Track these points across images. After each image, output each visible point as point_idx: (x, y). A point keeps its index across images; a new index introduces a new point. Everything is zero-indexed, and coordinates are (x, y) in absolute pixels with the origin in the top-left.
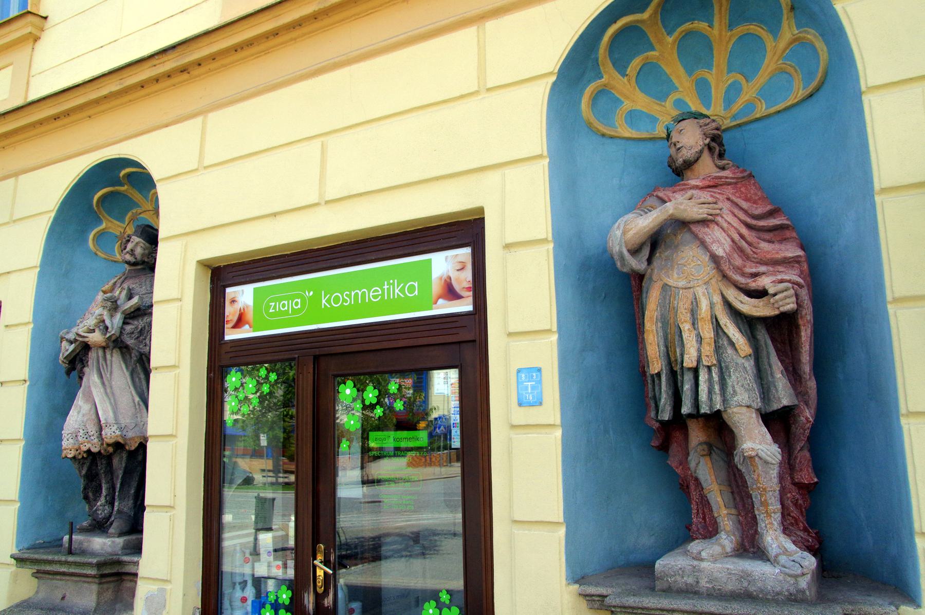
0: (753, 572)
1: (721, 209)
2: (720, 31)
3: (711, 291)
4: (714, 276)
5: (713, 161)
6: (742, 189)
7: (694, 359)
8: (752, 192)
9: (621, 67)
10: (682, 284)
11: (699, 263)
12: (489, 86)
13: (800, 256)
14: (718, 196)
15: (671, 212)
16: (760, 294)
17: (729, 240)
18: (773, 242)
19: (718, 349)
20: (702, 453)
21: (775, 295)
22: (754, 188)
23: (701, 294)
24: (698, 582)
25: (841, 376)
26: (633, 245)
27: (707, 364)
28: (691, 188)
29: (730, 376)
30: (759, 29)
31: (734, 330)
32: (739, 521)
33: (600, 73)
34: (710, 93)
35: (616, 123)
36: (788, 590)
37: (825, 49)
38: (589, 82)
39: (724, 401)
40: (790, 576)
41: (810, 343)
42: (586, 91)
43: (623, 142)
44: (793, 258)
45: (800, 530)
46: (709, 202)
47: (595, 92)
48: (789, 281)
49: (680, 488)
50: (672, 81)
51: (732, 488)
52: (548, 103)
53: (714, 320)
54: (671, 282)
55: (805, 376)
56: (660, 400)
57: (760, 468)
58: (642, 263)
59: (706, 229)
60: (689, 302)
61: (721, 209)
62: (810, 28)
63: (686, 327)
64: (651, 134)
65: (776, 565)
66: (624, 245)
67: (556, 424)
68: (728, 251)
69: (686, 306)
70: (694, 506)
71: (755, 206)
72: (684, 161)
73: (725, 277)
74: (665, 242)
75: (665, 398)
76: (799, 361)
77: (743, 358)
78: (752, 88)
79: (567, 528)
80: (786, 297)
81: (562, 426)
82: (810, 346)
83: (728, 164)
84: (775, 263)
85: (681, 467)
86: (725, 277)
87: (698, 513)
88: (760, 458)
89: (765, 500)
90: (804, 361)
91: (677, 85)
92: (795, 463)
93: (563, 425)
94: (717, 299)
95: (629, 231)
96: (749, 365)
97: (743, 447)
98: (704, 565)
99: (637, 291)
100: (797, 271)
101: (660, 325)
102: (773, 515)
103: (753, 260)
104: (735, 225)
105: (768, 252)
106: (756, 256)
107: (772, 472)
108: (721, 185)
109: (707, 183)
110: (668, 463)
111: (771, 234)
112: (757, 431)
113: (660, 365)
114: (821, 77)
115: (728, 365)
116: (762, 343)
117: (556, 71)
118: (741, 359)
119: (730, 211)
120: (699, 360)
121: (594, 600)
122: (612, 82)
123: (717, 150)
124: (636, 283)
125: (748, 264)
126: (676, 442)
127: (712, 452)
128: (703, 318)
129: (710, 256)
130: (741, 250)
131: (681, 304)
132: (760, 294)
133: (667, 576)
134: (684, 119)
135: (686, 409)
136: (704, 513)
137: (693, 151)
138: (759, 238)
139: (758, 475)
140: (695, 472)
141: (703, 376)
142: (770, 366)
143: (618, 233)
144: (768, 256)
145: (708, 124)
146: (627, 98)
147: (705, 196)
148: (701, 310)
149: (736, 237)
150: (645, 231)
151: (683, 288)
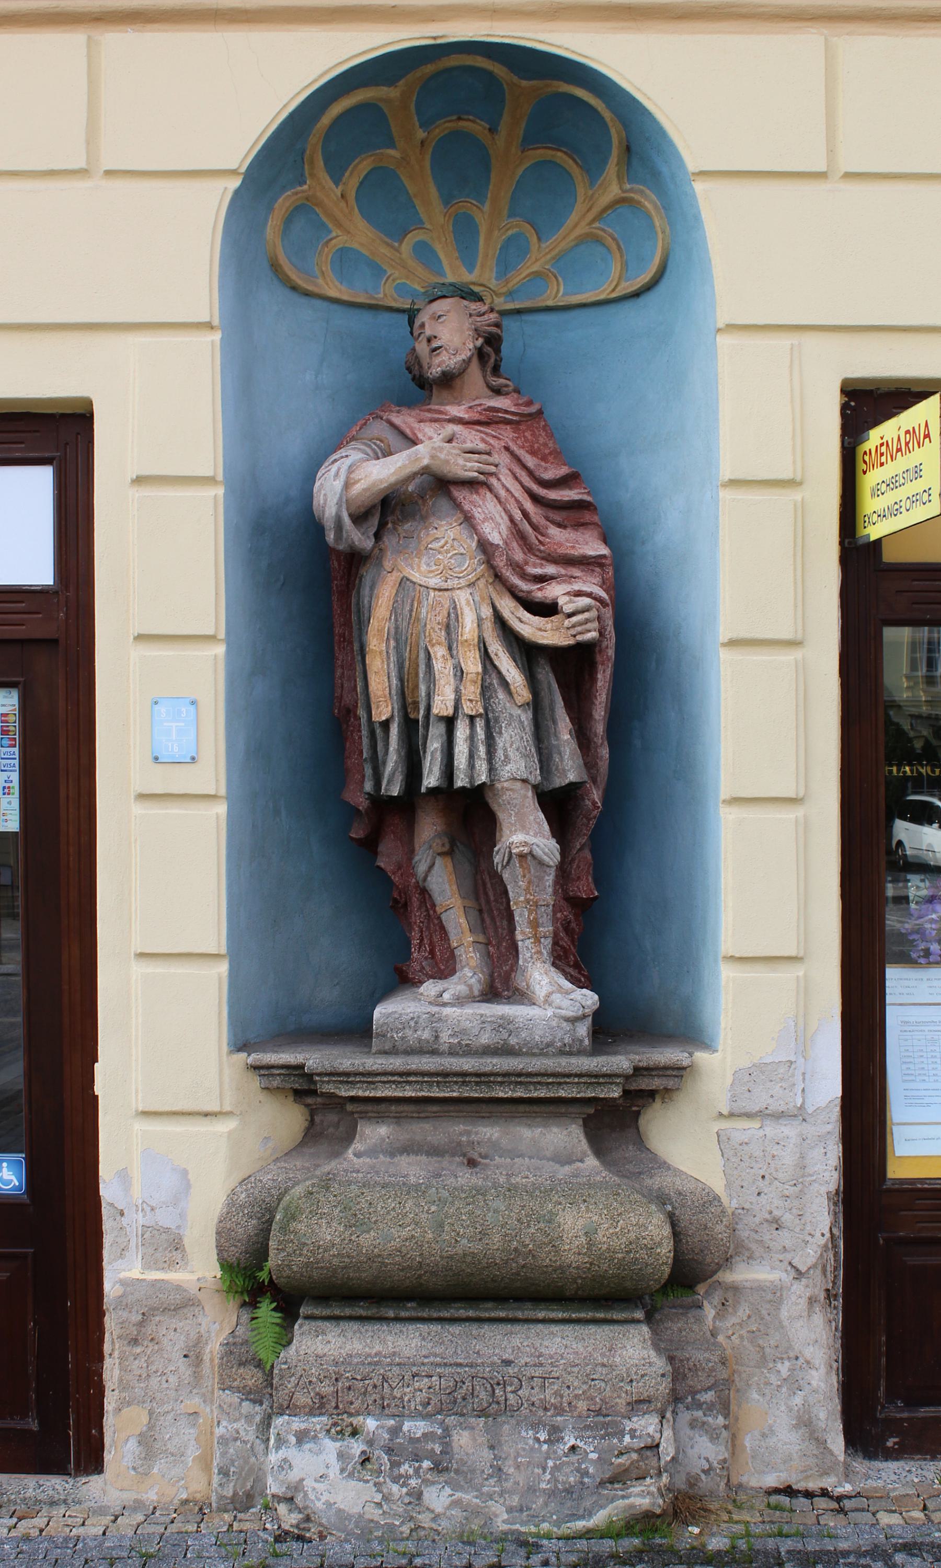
4: (483, 575)
5: (484, 377)
6: (526, 434)
8: (541, 440)
9: (337, 174)
10: (434, 582)
11: (462, 551)
13: (604, 556)
14: (492, 441)
15: (426, 462)
16: (547, 609)
17: (506, 518)
18: (565, 527)
19: (486, 691)
20: (440, 850)
21: (570, 616)
23: (463, 602)
24: (437, 1037)
25: (637, 743)
26: (359, 507)
27: (470, 713)
29: (500, 733)
30: (571, 162)
33: (302, 175)
34: (477, 242)
36: (562, 1040)
37: (600, 102)
39: (491, 769)
41: (608, 690)
43: (325, 304)
44: (594, 557)
45: (570, 966)
47: (291, 209)
48: (589, 595)
51: (480, 905)
52: (224, 227)
53: (482, 645)
54: (416, 576)
55: (595, 739)
56: (384, 763)
58: (368, 537)
61: (496, 466)
64: (373, 298)
66: (344, 506)
67: (219, 794)
68: (505, 537)
69: (439, 618)
71: (543, 464)
72: (444, 373)
73: (498, 577)
75: (396, 762)
76: (590, 716)
77: (520, 707)
78: (547, 254)
79: (230, 964)
81: (227, 798)
82: (607, 695)
83: (507, 386)
87: (421, 944)
88: (533, 856)
90: (597, 717)
91: (423, 216)
94: (487, 612)
96: (527, 718)
100: (598, 580)
102: (542, 940)
103: (538, 553)
104: (517, 495)
106: (542, 548)
107: (547, 878)
109: (476, 417)
110: (378, 867)
111: (564, 514)
112: (532, 818)
113: (390, 708)
115: (499, 717)
116: (545, 686)
117: (243, 169)
119: (510, 470)
120: (457, 706)
121: (273, 1075)
123: (492, 360)
124: (339, 565)
125: (533, 559)
127: (455, 848)
128: (466, 641)
129: (479, 541)
130: (521, 536)
132: (547, 609)
134: (444, 297)
135: (431, 779)
136: (431, 944)
137: (460, 358)
138: (547, 519)
140: (425, 879)
141: (461, 731)
143: (338, 484)
144: (561, 551)
145: (484, 314)
146: (339, 225)
147: (472, 438)
149: (518, 515)
150: (382, 486)
151: (435, 589)
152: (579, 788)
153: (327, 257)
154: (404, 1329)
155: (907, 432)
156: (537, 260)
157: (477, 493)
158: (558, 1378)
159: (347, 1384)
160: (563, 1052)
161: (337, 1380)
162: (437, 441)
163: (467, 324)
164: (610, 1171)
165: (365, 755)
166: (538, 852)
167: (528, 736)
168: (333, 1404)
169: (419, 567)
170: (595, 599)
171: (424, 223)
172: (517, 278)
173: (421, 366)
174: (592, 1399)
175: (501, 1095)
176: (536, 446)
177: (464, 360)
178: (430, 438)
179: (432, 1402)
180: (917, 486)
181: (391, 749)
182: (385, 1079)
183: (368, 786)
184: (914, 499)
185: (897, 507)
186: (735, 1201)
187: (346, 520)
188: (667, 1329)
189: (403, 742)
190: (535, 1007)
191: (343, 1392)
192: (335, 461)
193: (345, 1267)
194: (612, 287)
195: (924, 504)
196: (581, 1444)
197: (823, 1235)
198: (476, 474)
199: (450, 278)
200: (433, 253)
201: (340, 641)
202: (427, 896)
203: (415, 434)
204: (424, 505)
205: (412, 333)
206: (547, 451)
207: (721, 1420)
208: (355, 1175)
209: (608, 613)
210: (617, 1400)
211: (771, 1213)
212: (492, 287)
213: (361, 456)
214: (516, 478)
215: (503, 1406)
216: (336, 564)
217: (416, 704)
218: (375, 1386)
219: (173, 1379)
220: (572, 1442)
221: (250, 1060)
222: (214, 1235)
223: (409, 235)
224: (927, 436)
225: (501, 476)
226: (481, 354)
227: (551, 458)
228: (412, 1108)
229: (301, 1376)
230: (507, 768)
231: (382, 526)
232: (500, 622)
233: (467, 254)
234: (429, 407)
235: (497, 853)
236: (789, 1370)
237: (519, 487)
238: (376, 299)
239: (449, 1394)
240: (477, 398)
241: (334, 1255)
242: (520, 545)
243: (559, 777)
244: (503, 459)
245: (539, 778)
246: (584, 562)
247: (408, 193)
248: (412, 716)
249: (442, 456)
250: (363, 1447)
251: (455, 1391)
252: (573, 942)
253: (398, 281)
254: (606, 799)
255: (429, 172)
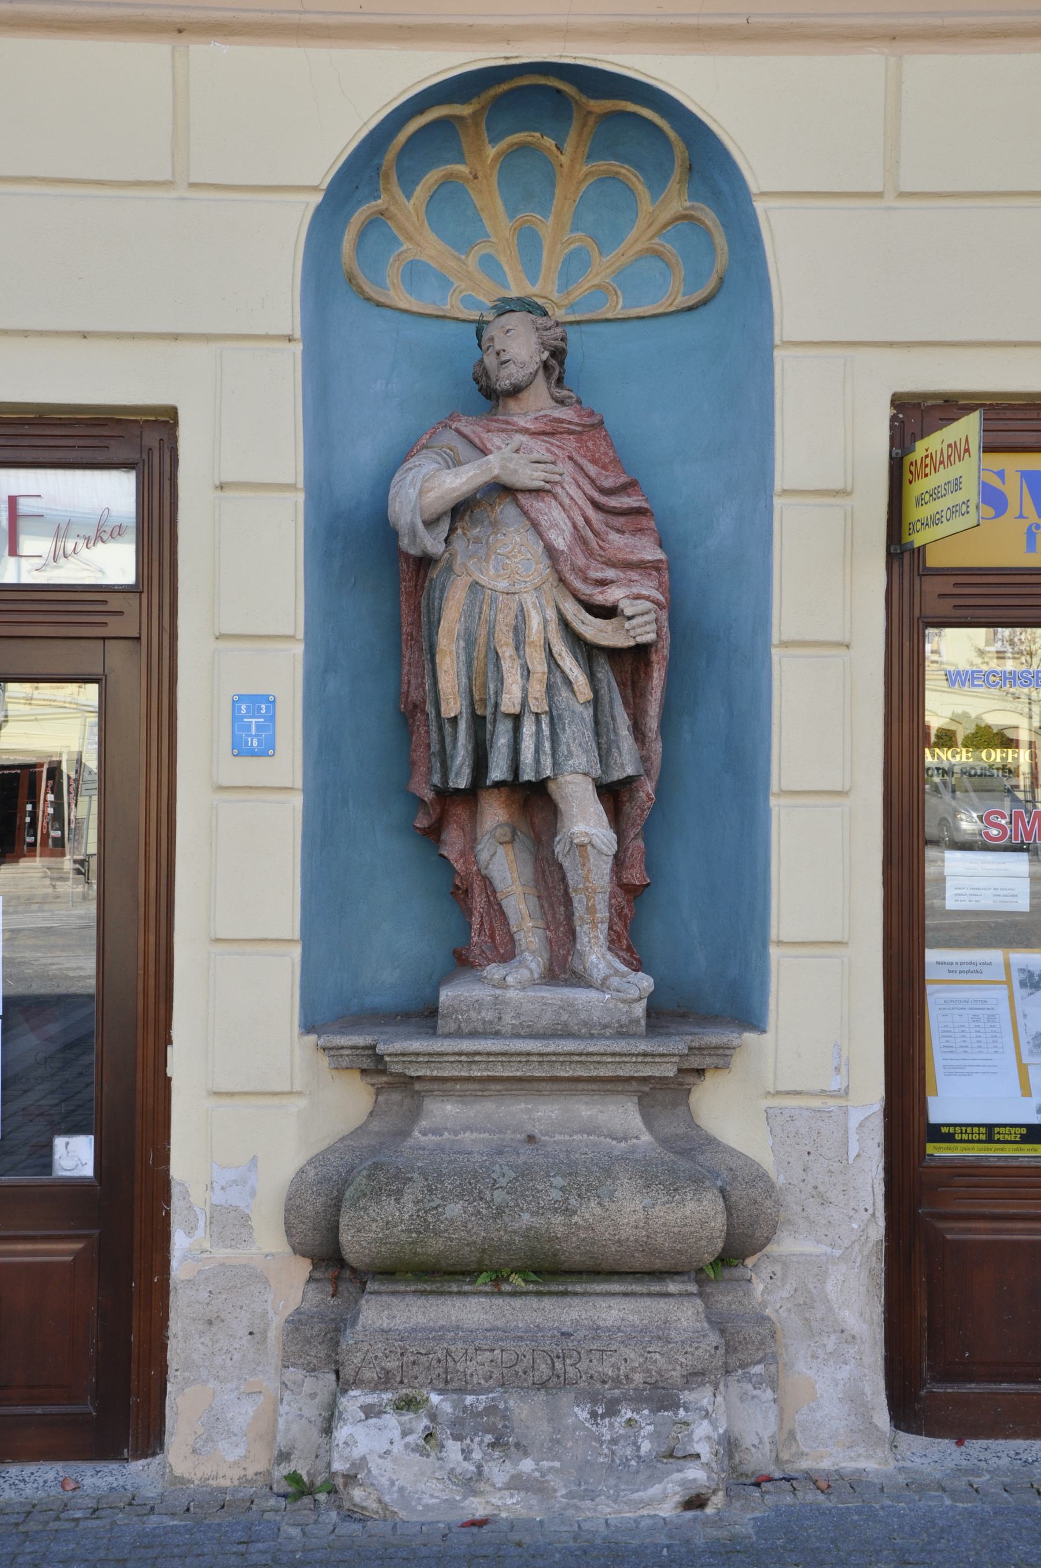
0: (576, 999)
1: (561, 475)
2: (573, 161)
3: (544, 601)
5: (549, 389)
6: (588, 444)
7: (518, 701)
8: (602, 449)
10: (502, 585)
12: (194, 179)
13: (660, 561)
15: (496, 472)
16: (608, 612)
17: (569, 524)
18: (623, 532)
21: (630, 618)
22: (604, 443)
23: (530, 605)
24: (500, 1018)
27: (536, 710)
28: (517, 431)
29: (564, 729)
31: (571, 664)
32: (547, 937)
33: (377, 190)
35: (388, 280)
36: (618, 1021)
38: (360, 203)
40: (624, 1001)
41: (663, 688)
42: (352, 220)
45: (623, 950)
46: (546, 460)
47: (366, 223)
48: (647, 598)
49: (452, 893)
50: (481, 220)
53: (547, 646)
54: (483, 580)
55: (650, 734)
56: (453, 757)
57: (592, 860)
59: (541, 504)
60: (513, 615)
61: (561, 475)
62: (708, 206)
63: (507, 652)
65: (605, 989)
70: (476, 920)
71: (603, 472)
73: (562, 580)
74: (472, 512)
78: (607, 268)
80: (647, 623)
83: (570, 397)
84: (628, 566)
85: (462, 860)
86: (562, 580)
89: (594, 905)
91: (489, 229)
92: (625, 856)
93: (305, 790)
94: (551, 614)
95: (430, 491)
97: (572, 831)
98: (511, 994)
99: (410, 580)
101: (462, 643)
103: (599, 558)
105: (620, 549)
108: (561, 433)
111: (622, 520)
112: (592, 810)
114: (714, 288)
117: (325, 186)
118: (579, 705)
119: (573, 478)
122: (392, 208)
123: (557, 373)
124: (408, 567)
125: (594, 564)
126: (456, 822)
130: (583, 541)
131: (500, 617)
132: (608, 612)
133: (457, 1011)
135: (498, 771)
139: (589, 871)
140: (486, 868)
141: (528, 729)
142: (613, 719)
143: (413, 493)
144: (620, 556)
145: (550, 328)
146: (410, 238)
147: (539, 448)
148: (530, 629)
149: (580, 522)
150: (455, 495)
152: (636, 781)
153: (398, 270)
154: (467, 1304)
155: (950, 446)
156: (597, 274)
157: (543, 501)
158: (616, 1351)
159: (412, 1359)
160: (622, 1034)
161: (402, 1354)
162: (507, 451)
163: (534, 338)
164: (664, 1148)
165: (432, 749)
166: (597, 841)
167: (589, 734)
168: (398, 1379)
169: (487, 570)
170: (653, 602)
171: (490, 237)
172: (580, 290)
173: (488, 377)
174: (649, 1371)
175: (563, 1074)
176: (597, 455)
177: (531, 373)
178: (499, 448)
179: (494, 1376)
180: (958, 498)
181: (459, 744)
182: (453, 1059)
183: (436, 779)
184: (954, 511)
185: (938, 516)
186: (782, 1177)
187: (420, 526)
188: (717, 1301)
189: (470, 737)
190: (591, 989)
191: (408, 1367)
192: (411, 469)
193: (413, 1243)
194: (670, 301)
195: (963, 515)
196: (637, 1417)
197: (866, 1210)
198: (543, 483)
199: (514, 293)
200: (499, 267)
201: (407, 640)
202: (488, 883)
203: (483, 444)
204: (492, 512)
205: (480, 345)
206: (607, 460)
207: (769, 1394)
208: (421, 1152)
209: (664, 616)
210: (673, 1373)
211: (816, 1188)
212: (554, 300)
213: (435, 466)
214: (579, 487)
215: (562, 1379)
216: (405, 566)
217: (484, 702)
218: (439, 1361)
219: (237, 1356)
220: (629, 1415)
221: (322, 1042)
222: (284, 1212)
223: (476, 248)
224: (967, 450)
225: (565, 485)
226: (546, 366)
227: (610, 467)
228: (476, 1086)
229: (368, 1351)
230: (570, 762)
231: (452, 530)
232: (565, 625)
233: (531, 269)
234: (496, 417)
235: (558, 843)
236: (835, 1344)
237: (581, 495)
238: (444, 310)
239: (510, 1367)
240: (542, 409)
241: (402, 1231)
242: (582, 551)
243: (617, 771)
244: (567, 468)
245: (599, 772)
246: (641, 566)
247: (475, 206)
248: (479, 712)
249: (512, 466)
250: (425, 1422)
251: (516, 1364)
252: (625, 926)
253: (464, 293)
254: (657, 790)
255: (496, 186)
